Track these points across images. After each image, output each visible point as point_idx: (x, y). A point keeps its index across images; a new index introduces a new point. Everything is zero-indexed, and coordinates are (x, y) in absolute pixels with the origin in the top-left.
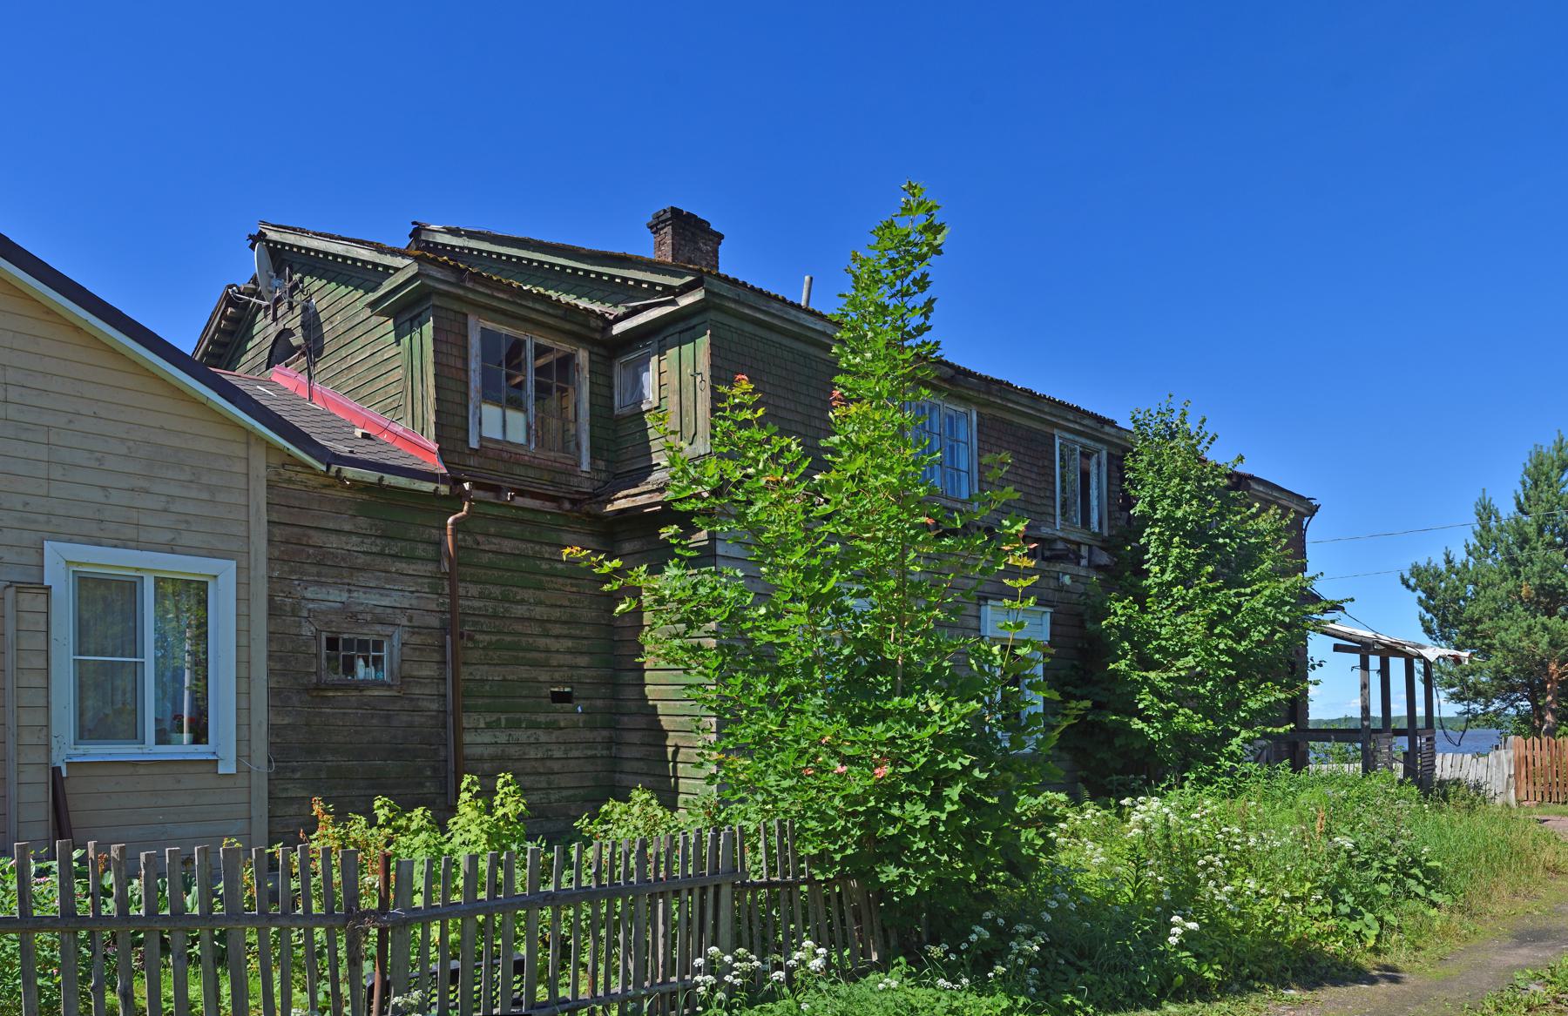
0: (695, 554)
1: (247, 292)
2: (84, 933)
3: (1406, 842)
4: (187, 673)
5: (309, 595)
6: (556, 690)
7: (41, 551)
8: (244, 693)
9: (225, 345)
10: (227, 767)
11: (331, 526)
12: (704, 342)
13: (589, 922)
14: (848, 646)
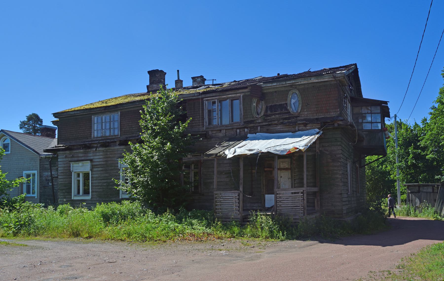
0: (415, 197)
1: (405, 203)
2: (146, 128)
3: (435, 130)
4: (418, 184)
5: (44, 174)
6: (179, 102)
7: (176, 86)
8: (37, 190)
9: (244, 222)
10: (36, 197)
11: (46, 164)
12: (227, 158)
13: (424, 178)
14: (411, 146)
